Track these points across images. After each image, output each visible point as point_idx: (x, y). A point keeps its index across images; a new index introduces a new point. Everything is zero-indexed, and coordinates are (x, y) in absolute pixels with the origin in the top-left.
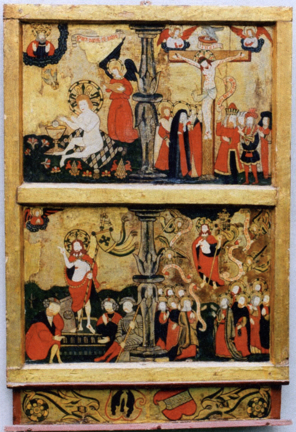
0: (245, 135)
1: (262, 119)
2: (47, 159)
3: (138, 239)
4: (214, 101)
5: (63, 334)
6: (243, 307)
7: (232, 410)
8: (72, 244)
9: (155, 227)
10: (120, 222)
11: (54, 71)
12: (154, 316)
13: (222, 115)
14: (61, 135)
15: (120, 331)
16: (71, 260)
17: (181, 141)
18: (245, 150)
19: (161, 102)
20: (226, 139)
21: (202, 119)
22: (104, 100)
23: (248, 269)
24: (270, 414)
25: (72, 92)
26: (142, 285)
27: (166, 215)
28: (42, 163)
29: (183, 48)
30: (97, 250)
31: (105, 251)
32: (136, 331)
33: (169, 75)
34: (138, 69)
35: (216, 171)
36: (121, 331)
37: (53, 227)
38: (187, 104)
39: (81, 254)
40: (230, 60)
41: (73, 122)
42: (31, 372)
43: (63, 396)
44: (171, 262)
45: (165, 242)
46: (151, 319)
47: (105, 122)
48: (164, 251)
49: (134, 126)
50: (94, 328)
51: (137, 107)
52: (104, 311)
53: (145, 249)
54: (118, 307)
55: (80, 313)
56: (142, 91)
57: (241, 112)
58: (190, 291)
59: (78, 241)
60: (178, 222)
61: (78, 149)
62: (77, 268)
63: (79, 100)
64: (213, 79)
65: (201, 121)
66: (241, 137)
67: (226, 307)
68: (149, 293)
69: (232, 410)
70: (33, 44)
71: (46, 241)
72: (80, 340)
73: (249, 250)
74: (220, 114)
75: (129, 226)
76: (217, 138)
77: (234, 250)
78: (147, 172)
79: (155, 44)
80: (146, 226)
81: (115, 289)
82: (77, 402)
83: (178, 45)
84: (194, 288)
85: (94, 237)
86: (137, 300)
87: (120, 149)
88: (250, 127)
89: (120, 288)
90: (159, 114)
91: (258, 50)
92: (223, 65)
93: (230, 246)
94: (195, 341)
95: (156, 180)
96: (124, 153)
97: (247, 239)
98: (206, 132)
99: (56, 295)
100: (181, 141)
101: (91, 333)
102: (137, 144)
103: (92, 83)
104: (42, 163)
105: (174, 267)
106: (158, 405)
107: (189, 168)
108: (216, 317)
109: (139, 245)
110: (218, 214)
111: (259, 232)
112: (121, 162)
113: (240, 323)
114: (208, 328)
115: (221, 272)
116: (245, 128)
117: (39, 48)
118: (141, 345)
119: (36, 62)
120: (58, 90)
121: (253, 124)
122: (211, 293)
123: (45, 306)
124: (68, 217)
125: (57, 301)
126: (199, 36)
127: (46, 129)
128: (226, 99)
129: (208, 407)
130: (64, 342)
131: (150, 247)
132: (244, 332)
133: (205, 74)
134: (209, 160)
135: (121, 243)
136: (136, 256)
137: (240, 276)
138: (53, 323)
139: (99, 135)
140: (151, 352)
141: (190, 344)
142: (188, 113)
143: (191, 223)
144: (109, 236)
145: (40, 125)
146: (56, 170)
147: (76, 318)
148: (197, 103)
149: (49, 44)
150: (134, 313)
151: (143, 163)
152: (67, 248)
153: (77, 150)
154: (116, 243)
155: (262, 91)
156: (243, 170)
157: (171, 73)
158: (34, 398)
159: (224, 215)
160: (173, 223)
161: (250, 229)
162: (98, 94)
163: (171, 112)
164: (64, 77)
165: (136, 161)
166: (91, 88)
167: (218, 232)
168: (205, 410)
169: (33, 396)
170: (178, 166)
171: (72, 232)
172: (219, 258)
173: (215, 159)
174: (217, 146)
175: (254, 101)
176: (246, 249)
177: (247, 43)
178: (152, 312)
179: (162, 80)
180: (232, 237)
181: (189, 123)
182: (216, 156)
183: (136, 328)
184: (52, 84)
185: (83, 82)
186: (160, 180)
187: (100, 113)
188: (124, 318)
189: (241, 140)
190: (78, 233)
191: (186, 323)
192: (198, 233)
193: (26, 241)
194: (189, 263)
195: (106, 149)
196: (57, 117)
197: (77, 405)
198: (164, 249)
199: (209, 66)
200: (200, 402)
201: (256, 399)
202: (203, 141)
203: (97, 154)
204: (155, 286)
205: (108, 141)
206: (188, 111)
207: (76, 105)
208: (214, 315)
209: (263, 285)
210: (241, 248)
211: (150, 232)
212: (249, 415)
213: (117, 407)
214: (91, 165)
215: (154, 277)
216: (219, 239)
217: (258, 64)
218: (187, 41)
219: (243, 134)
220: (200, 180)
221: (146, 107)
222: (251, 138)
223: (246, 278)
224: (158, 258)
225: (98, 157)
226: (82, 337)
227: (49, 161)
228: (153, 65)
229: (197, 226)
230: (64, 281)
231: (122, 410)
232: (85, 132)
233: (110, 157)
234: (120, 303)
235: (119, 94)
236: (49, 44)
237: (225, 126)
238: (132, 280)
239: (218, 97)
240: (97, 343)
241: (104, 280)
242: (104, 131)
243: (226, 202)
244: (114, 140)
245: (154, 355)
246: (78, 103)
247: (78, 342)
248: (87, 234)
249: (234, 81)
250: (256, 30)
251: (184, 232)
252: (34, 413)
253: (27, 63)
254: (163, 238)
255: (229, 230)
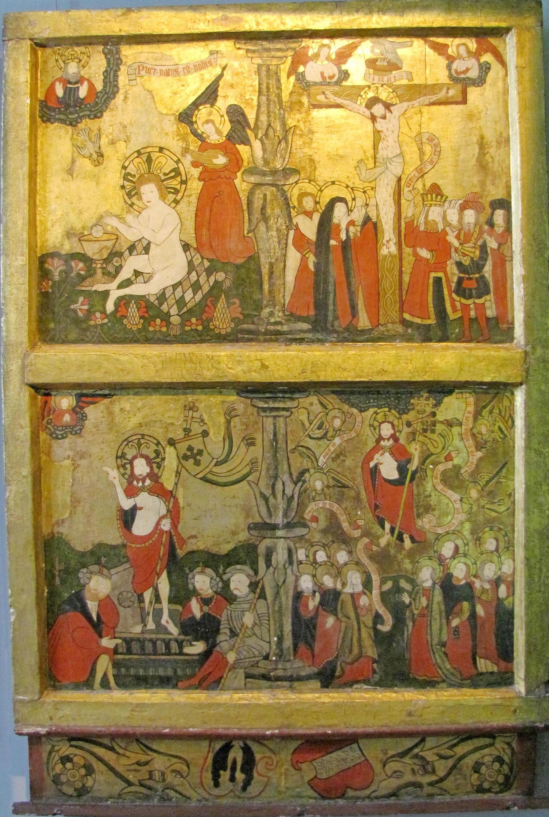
0: (461, 244)
1: (492, 214)
2: (81, 299)
3: (256, 451)
4: (399, 180)
5: (117, 635)
6: (463, 582)
7: (441, 780)
8: (131, 463)
9: (289, 429)
10: (222, 420)
11: (96, 132)
12: (290, 603)
13: (415, 206)
14: (109, 251)
15: (224, 629)
16: (130, 492)
17: (335, 257)
18: (461, 275)
19: (296, 183)
20: (424, 253)
21: (378, 216)
22: (189, 183)
23: (471, 508)
24: (515, 785)
25: (128, 170)
26: (267, 542)
27: (311, 404)
28: (72, 307)
29: (338, 80)
30: (178, 473)
31: (195, 476)
32: (257, 630)
33: (311, 132)
34: (252, 122)
35: (407, 316)
36: (227, 631)
37: (94, 430)
38: (347, 187)
39: (148, 482)
40: (427, 102)
41: (130, 227)
42: (57, 705)
43: (121, 751)
44: (322, 496)
45: (309, 457)
46: (283, 608)
47: (190, 225)
48: (307, 475)
49: (246, 232)
50: (176, 625)
51: (251, 193)
52: (195, 592)
53: (271, 472)
54: (220, 585)
55: (148, 595)
56: (260, 163)
57: (451, 201)
58: (358, 552)
59: (142, 456)
60: (335, 417)
61: (140, 278)
62: (141, 509)
63: (142, 184)
64: (396, 140)
65: (374, 220)
66: (453, 250)
67: (428, 584)
68: (280, 556)
69: (441, 780)
70: (57, 83)
71: (82, 457)
72: (149, 646)
73: (472, 472)
74: (412, 205)
75: (239, 427)
76: (407, 251)
77: (444, 473)
78: (272, 320)
79: (283, 76)
80: (272, 427)
81: (214, 550)
82: (147, 763)
83: (326, 75)
84: (367, 548)
85: (172, 448)
86: (256, 572)
87: (220, 276)
88: (469, 230)
89: (225, 548)
90: (294, 207)
91: (480, 81)
92: (413, 110)
93: (435, 464)
94: (371, 651)
95: (290, 336)
96: (228, 283)
97: (470, 450)
98: (384, 241)
99: (103, 560)
100: (335, 257)
101: (170, 634)
102: (252, 266)
103: (165, 151)
104: (72, 307)
105: (328, 506)
106: (300, 769)
107: (354, 313)
108: (410, 604)
109: (260, 464)
110: (412, 401)
111: (493, 435)
112: (222, 303)
113: (458, 615)
114: (394, 626)
115: (419, 516)
116: (460, 230)
117: (67, 91)
118: (267, 657)
119: (62, 117)
120: (102, 166)
121: (476, 225)
122: (400, 557)
123: (82, 581)
124: (121, 409)
125: (105, 571)
126: (368, 57)
127: (80, 240)
128: (422, 176)
129: (397, 773)
130: (120, 650)
131: (280, 468)
132: (466, 631)
133: (379, 128)
134: (394, 293)
135: (225, 461)
136: (253, 485)
137: (456, 523)
138: (98, 616)
139: (179, 249)
140: (285, 669)
141: (361, 655)
142: (350, 204)
143: (359, 419)
144: (201, 447)
145: (69, 234)
146: (98, 319)
147: (142, 605)
148: (368, 185)
149: (86, 83)
150: (251, 596)
151: (265, 302)
152: (122, 470)
153: (138, 279)
154: (215, 460)
155: (490, 160)
156: (459, 314)
157: (314, 129)
158: (67, 753)
159: (423, 401)
160: (324, 419)
161: (475, 431)
162: (177, 172)
163: (317, 203)
164: (113, 143)
165: (251, 298)
166: (163, 160)
167: (412, 437)
168: (391, 779)
169: (65, 749)
170: (331, 308)
171: (130, 439)
172: (414, 487)
173: (404, 292)
174: (407, 269)
175: (475, 180)
176: (465, 471)
177: (459, 70)
178: (287, 593)
179: (298, 142)
180: (441, 446)
181: (352, 223)
182: (405, 286)
183: (255, 624)
184: (91, 155)
185: (149, 150)
186: (298, 337)
187: (183, 205)
188: (232, 606)
189: (453, 254)
190: (142, 441)
191: (352, 615)
192: (374, 440)
193: (44, 458)
194: (357, 498)
195: (194, 276)
196: (101, 217)
197: (147, 768)
198: (308, 470)
199: (388, 115)
200: (380, 766)
201: (487, 759)
202: (380, 258)
203: (175, 287)
204: (292, 545)
205: (197, 260)
206: (349, 199)
207: (136, 193)
208: (406, 599)
209: (501, 538)
210: (457, 469)
211: (280, 437)
212: (475, 788)
213: (222, 772)
214: (165, 308)
215: (289, 526)
216: (415, 450)
217: (481, 107)
218: (344, 67)
219: (456, 243)
220: (375, 334)
221: (268, 193)
222: (473, 250)
223: (467, 526)
224: (297, 488)
225: (179, 293)
226: (154, 642)
227: (87, 302)
228: (280, 114)
229: (371, 425)
230: (117, 534)
231: (232, 779)
232: (152, 246)
233: (200, 292)
234: (225, 577)
235: (215, 171)
236: (86, 83)
237: (422, 228)
238: (246, 533)
239: (407, 172)
240: (181, 653)
241: (194, 533)
242: (189, 242)
243: (427, 378)
244: (207, 259)
245: (291, 676)
246: (139, 190)
247: (147, 652)
248: (159, 443)
249: (436, 141)
250: (475, 46)
251: (346, 437)
252: (69, 780)
253: (45, 119)
254: (304, 450)
255: (433, 431)
